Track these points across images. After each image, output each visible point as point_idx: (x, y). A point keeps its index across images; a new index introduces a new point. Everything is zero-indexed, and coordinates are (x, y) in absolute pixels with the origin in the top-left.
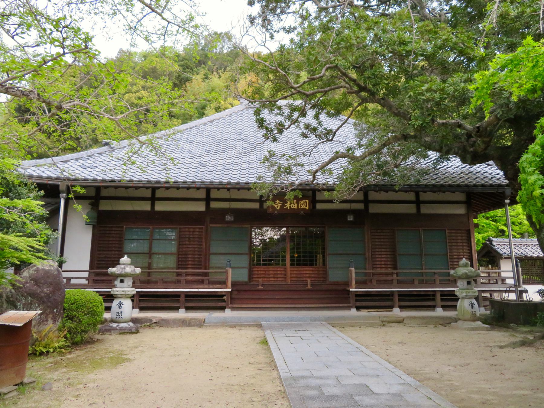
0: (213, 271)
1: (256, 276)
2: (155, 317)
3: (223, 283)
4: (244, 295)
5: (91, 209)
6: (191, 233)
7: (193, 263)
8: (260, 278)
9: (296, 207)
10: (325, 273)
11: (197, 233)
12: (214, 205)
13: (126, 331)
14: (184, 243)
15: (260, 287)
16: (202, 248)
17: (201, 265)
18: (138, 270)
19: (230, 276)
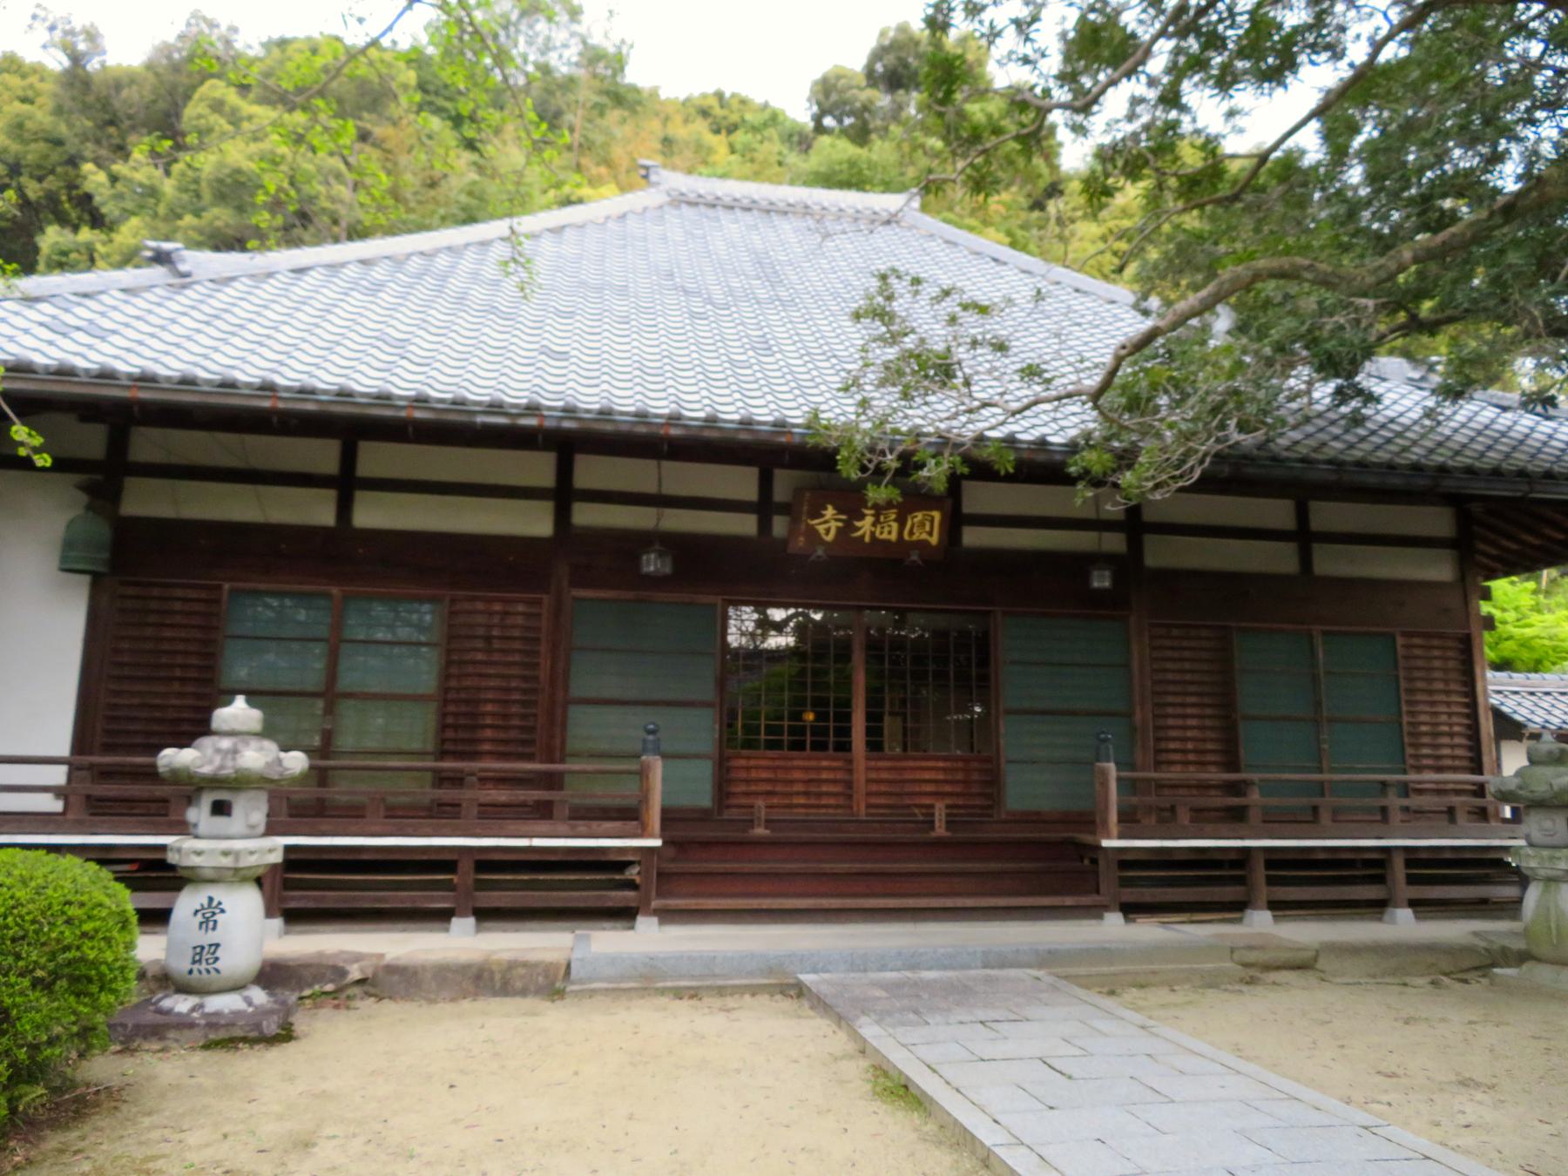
0: (576, 767)
1: (742, 788)
2: (358, 958)
3: (628, 815)
4: (710, 866)
5: (89, 508)
6: (496, 620)
7: (502, 735)
8: (756, 794)
9: (893, 537)
10: (993, 781)
11: (520, 620)
12: (586, 515)
13: (238, 1033)
14: (468, 657)
15: (760, 831)
16: (536, 678)
17: (531, 742)
18: (296, 761)
19: (658, 783)
